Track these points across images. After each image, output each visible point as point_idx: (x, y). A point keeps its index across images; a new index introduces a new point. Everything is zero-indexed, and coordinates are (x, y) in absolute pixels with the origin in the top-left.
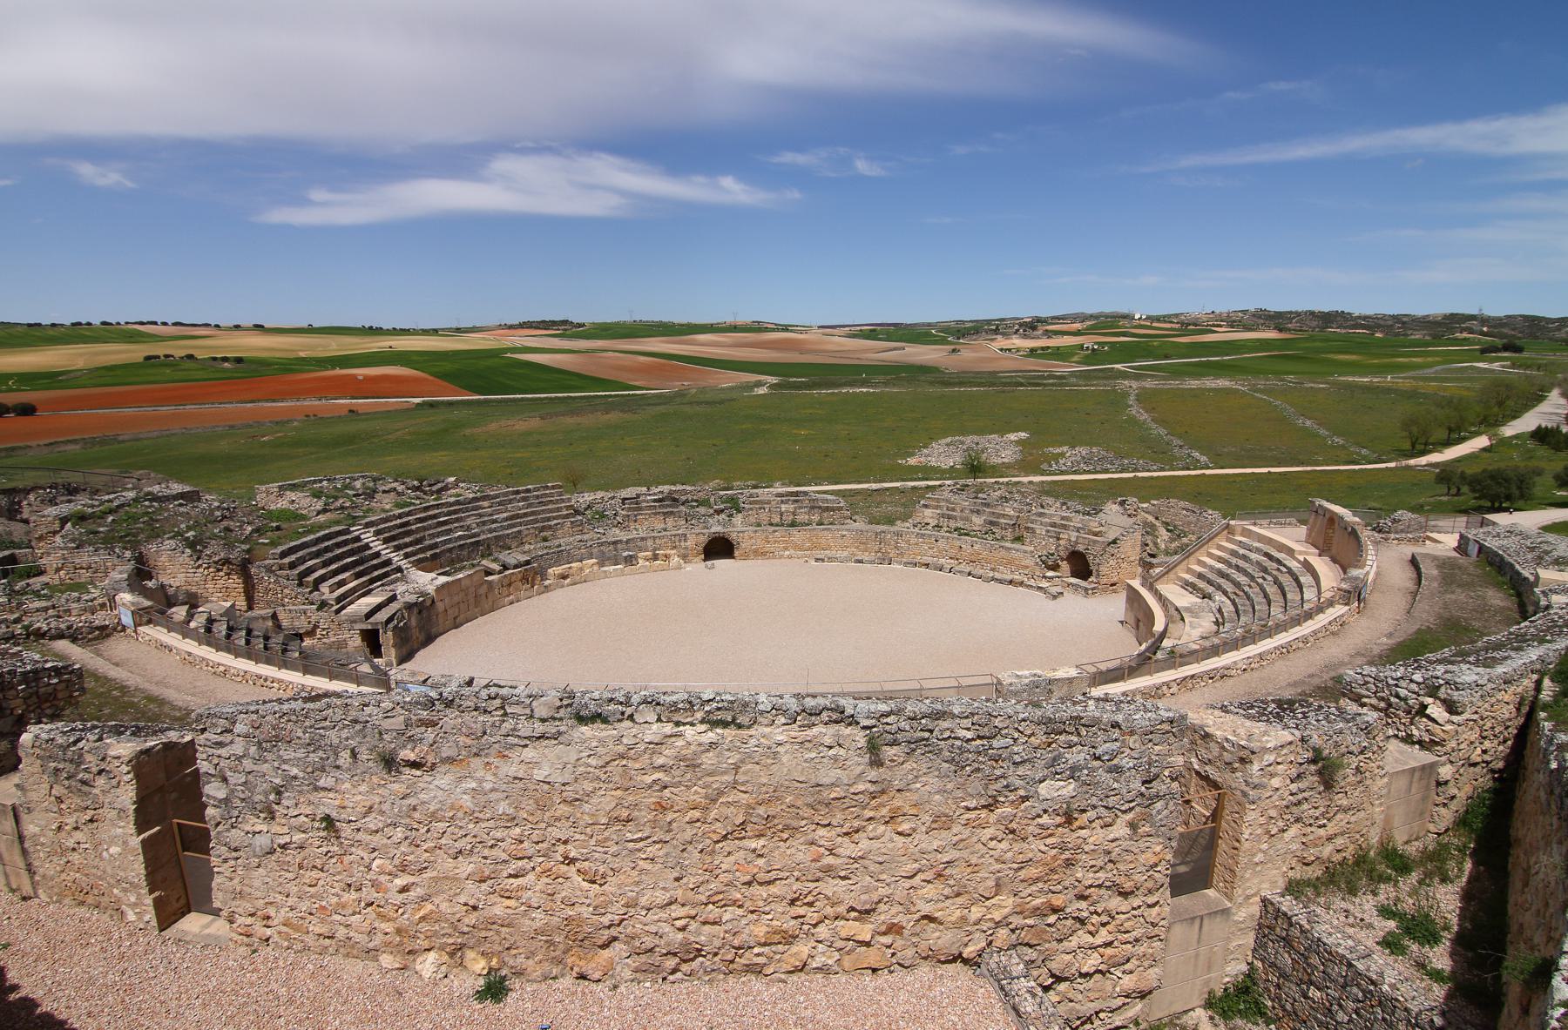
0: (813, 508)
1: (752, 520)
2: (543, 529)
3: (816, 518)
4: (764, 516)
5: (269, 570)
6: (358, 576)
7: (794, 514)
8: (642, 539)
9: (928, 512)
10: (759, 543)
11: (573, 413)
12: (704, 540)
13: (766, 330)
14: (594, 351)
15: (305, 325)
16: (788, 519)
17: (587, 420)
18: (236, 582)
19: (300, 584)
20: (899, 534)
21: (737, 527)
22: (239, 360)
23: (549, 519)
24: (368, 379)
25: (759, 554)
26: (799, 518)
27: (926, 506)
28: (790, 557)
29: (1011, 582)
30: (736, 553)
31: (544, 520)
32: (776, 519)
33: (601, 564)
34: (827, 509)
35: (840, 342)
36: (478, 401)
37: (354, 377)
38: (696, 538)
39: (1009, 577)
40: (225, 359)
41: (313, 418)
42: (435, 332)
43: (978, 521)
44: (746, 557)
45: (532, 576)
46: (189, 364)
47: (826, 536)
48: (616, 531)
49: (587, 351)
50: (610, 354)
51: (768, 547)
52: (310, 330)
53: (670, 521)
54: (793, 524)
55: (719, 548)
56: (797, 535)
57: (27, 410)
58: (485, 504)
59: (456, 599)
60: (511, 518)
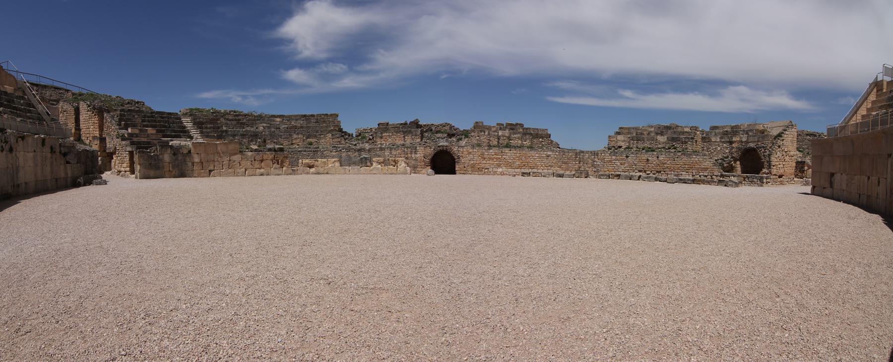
5: (113, 117)
7: (509, 138)
12: (430, 151)
18: (96, 119)
25: (477, 169)
28: (502, 174)
38: (423, 152)
56: (509, 154)
58: (278, 119)
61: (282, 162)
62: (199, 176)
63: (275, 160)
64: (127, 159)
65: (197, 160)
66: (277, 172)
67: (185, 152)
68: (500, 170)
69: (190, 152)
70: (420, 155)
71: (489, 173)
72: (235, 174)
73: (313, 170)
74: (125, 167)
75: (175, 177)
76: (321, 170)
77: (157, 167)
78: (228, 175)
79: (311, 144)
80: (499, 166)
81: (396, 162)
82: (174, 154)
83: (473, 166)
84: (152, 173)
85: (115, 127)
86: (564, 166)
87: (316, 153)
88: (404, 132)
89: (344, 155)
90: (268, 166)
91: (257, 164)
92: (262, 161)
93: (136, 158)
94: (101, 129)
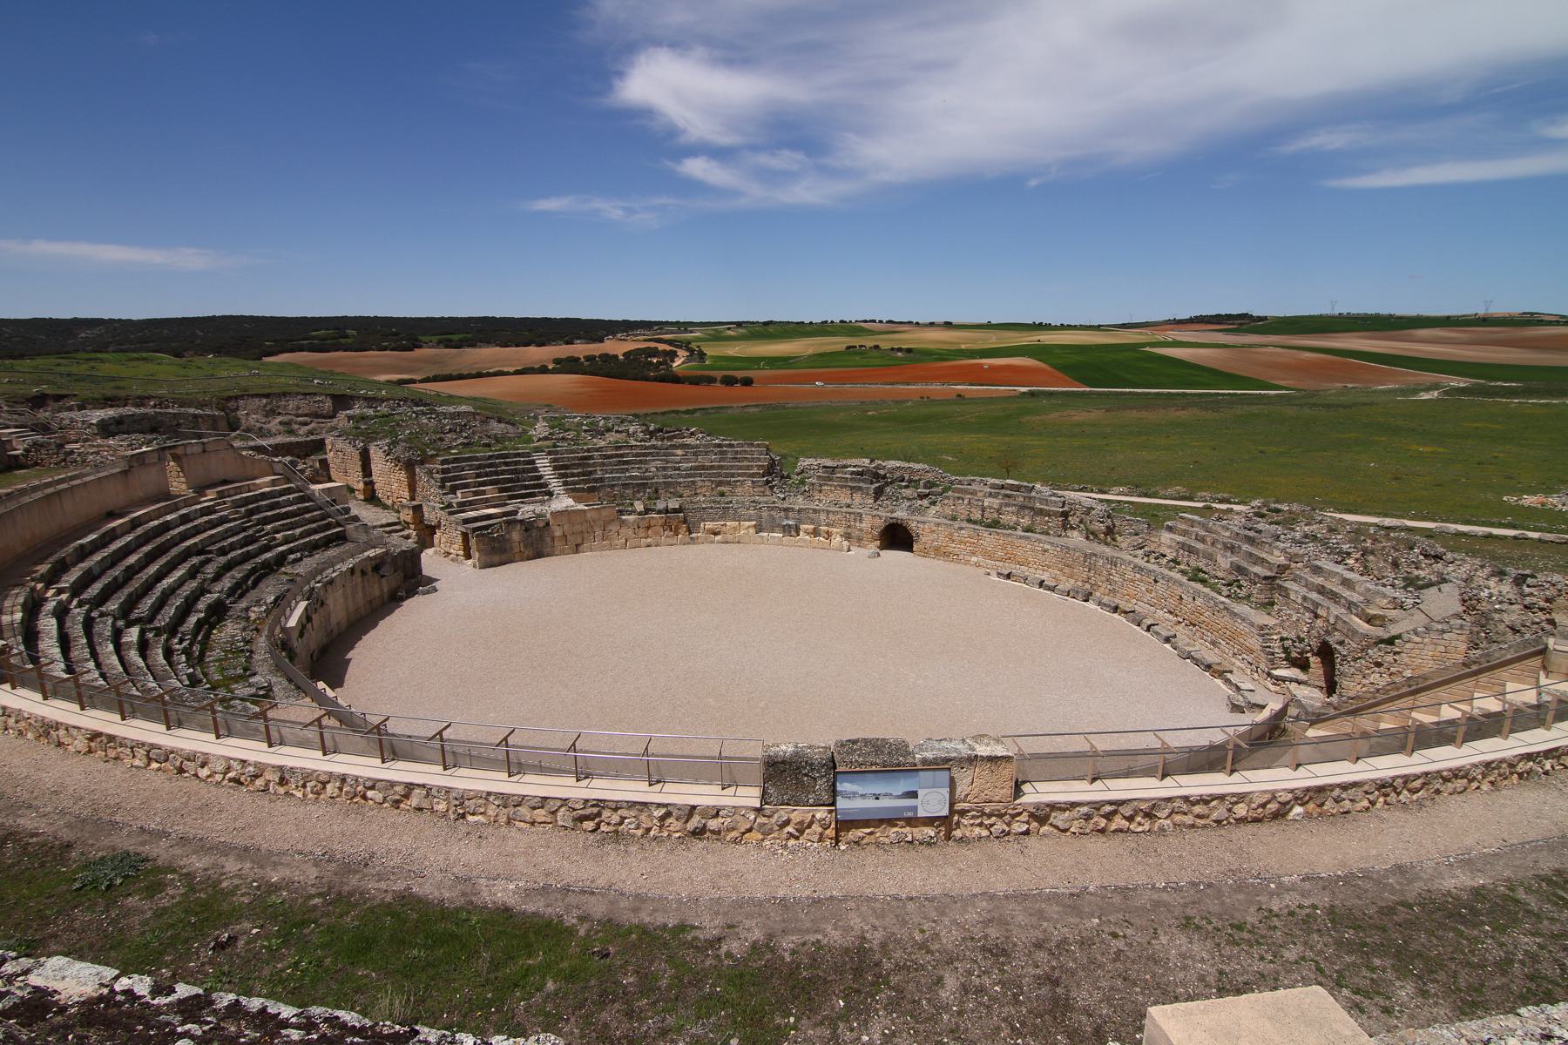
0: (1023, 507)
1: (948, 511)
2: (720, 484)
3: (1026, 521)
4: (962, 509)
5: (430, 473)
6: (501, 490)
7: (999, 511)
8: (815, 511)
9: (1166, 537)
10: (941, 539)
11: (1146, 408)
12: (880, 524)
13: (1541, 323)
14: (1250, 346)
15: (941, 320)
16: (990, 516)
17: (1150, 416)
18: (403, 475)
19: (442, 487)
20: (1113, 562)
21: (927, 522)
22: (909, 351)
23: (733, 475)
24: (992, 368)
25: (941, 553)
26: (1005, 519)
27: (1170, 529)
28: (977, 565)
29: (1208, 667)
30: (915, 547)
31: (727, 475)
32: (977, 515)
33: (759, 529)
34: (1041, 512)
35: (611, 209)
36: (1091, 393)
37: (981, 366)
38: (873, 519)
39: (1211, 657)
40: (900, 350)
41: (926, 400)
42: (1098, 328)
43: (1224, 561)
44: (925, 553)
45: (681, 523)
46: (875, 353)
47: (1026, 547)
48: (800, 499)
49: (1243, 346)
50: (1271, 349)
51: (952, 547)
52: (989, 326)
53: (858, 497)
54: (995, 524)
55: (897, 537)
56: (989, 539)
57: (747, 382)
58: (679, 452)
59: (578, 528)
60: (696, 468)
61: (677, 528)
62: (563, 553)
63: (667, 526)
64: (460, 539)
65: (558, 533)
66: (670, 541)
67: (541, 524)
68: (974, 559)
69: (548, 524)
70: (865, 525)
71: (959, 561)
72: (612, 547)
73: (718, 538)
74: (457, 548)
75: (529, 559)
76: (730, 538)
77: (503, 551)
78: (602, 549)
79: (722, 495)
80: (973, 553)
81: (829, 534)
82: (526, 530)
83: (937, 549)
84: (496, 559)
85: (435, 490)
86: (1067, 570)
87: (725, 513)
88: (852, 488)
89: (765, 514)
90: (657, 533)
91: (642, 533)
92: (648, 528)
93: (473, 542)
94: (412, 488)
